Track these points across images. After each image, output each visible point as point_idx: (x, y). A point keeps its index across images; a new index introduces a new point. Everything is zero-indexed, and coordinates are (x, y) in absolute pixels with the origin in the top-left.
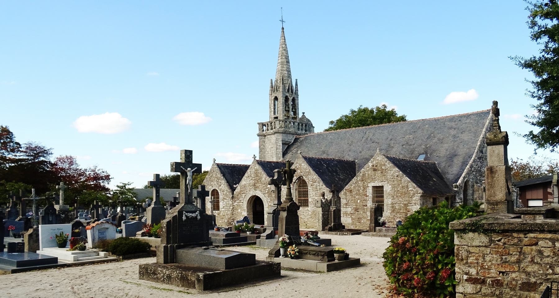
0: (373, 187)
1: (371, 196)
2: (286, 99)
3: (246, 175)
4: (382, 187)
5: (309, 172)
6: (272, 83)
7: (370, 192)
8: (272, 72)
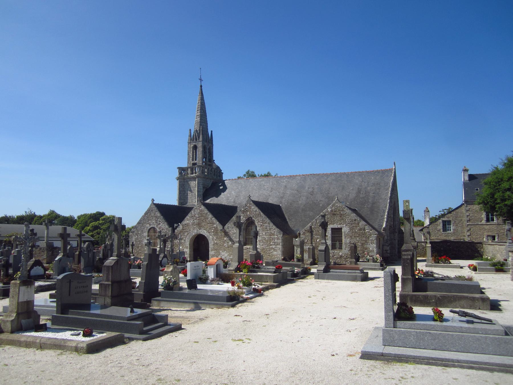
0: (332, 229)
2: (204, 147)
3: (190, 215)
4: (341, 229)
5: (207, 213)
8: (192, 123)
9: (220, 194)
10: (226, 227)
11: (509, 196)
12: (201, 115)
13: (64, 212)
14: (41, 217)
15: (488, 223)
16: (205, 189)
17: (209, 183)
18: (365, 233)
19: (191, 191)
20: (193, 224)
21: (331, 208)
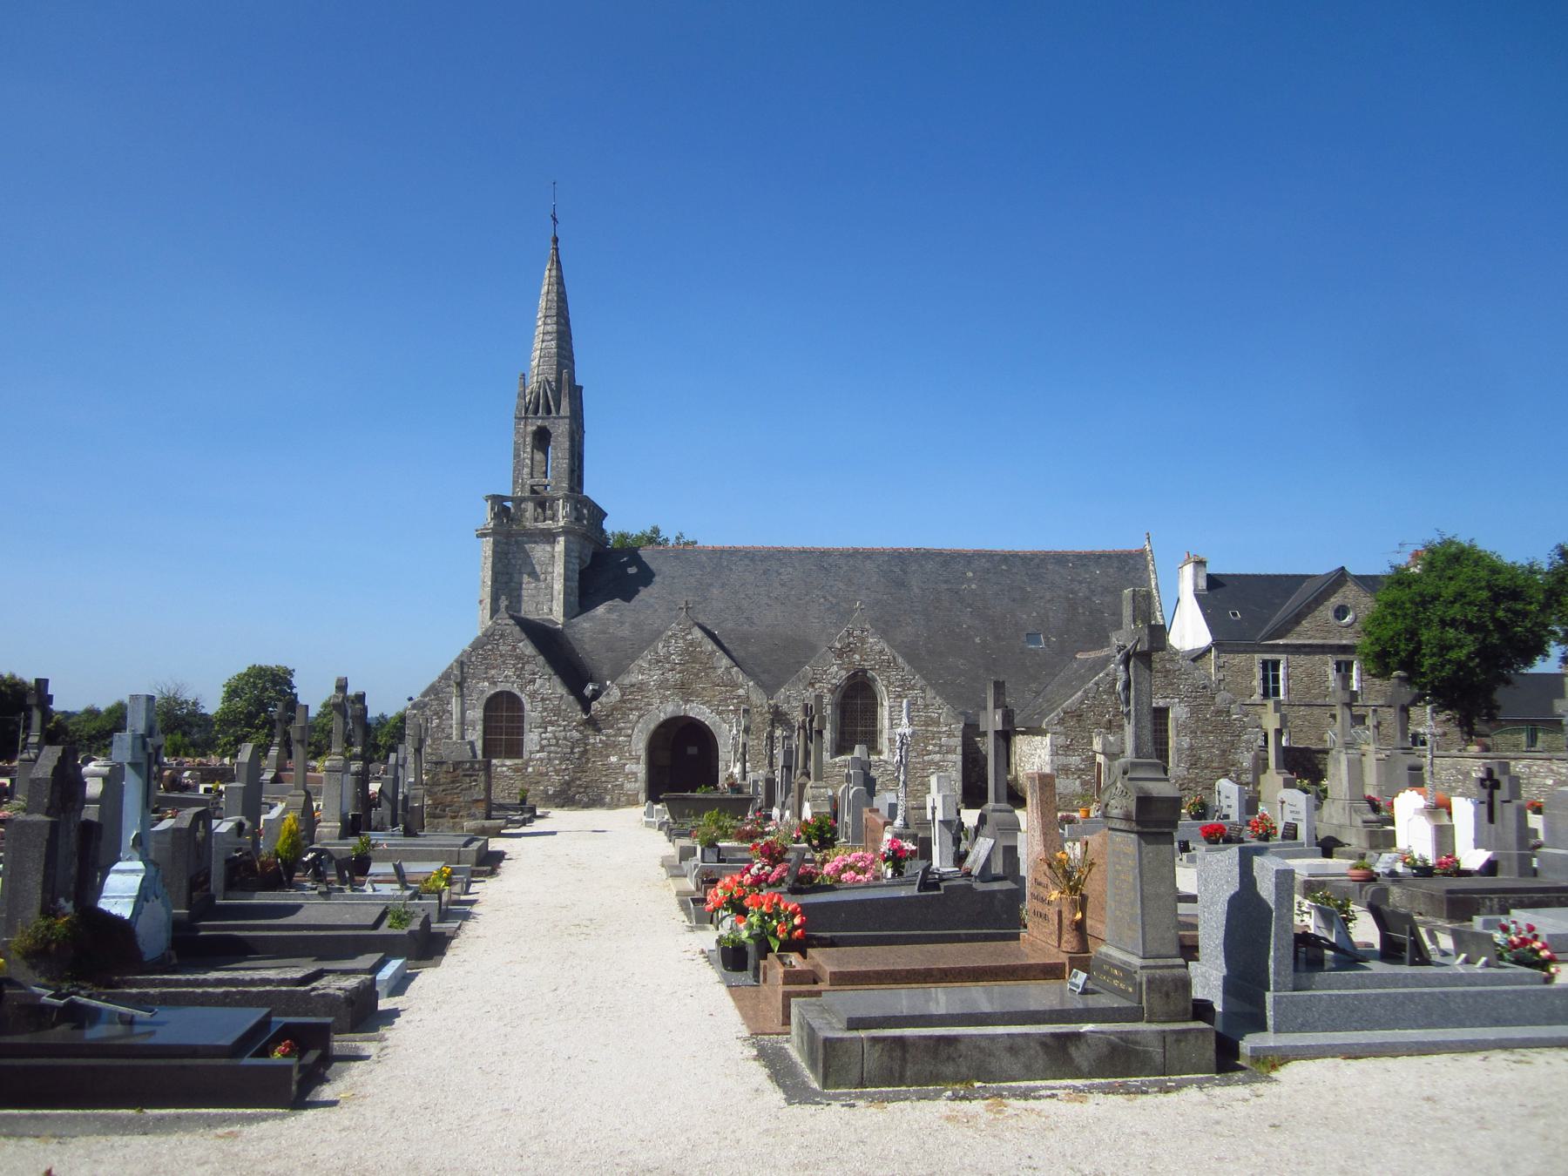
5: (714, 652)
9: (637, 592)
11: (1458, 640)
12: (558, 332)
18: (1230, 724)
19: (534, 575)
20: (662, 685)
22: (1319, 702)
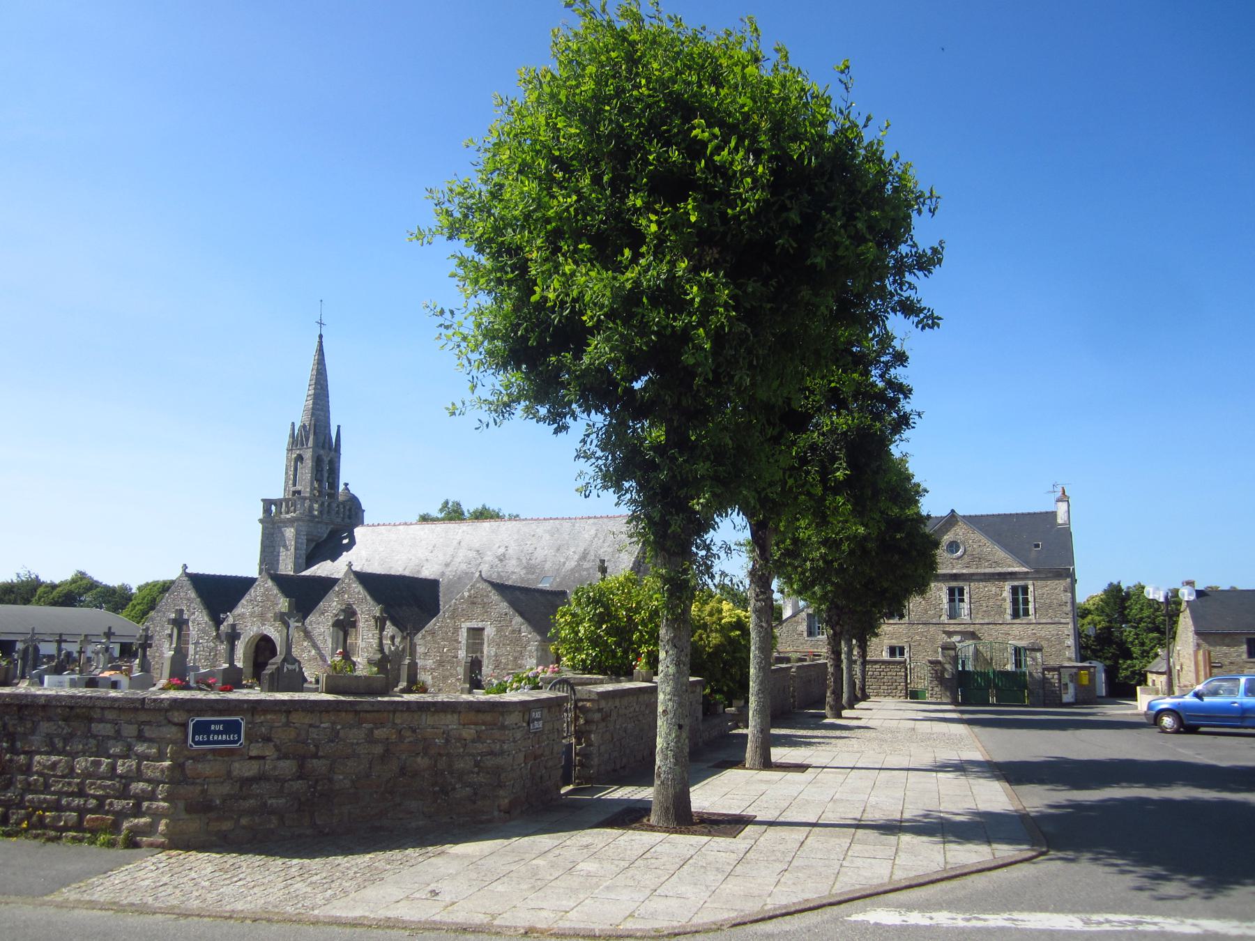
0: (469, 629)
1: (464, 642)
2: (318, 461)
3: (247, 597)
4: (483, 629)
6: (293, 429)
7: (463, 636)
8: (297, 412)
10: (307, 621)
12: (315, 394)
13: (109, 577)
14: (53, 587)
15: (952, 621)
16: (313, 545)
17: (324, 532)
18: (520, 639)
19: (285, 546)
20: (252, 615)
21: (469, 591)
22: (934, 621)
